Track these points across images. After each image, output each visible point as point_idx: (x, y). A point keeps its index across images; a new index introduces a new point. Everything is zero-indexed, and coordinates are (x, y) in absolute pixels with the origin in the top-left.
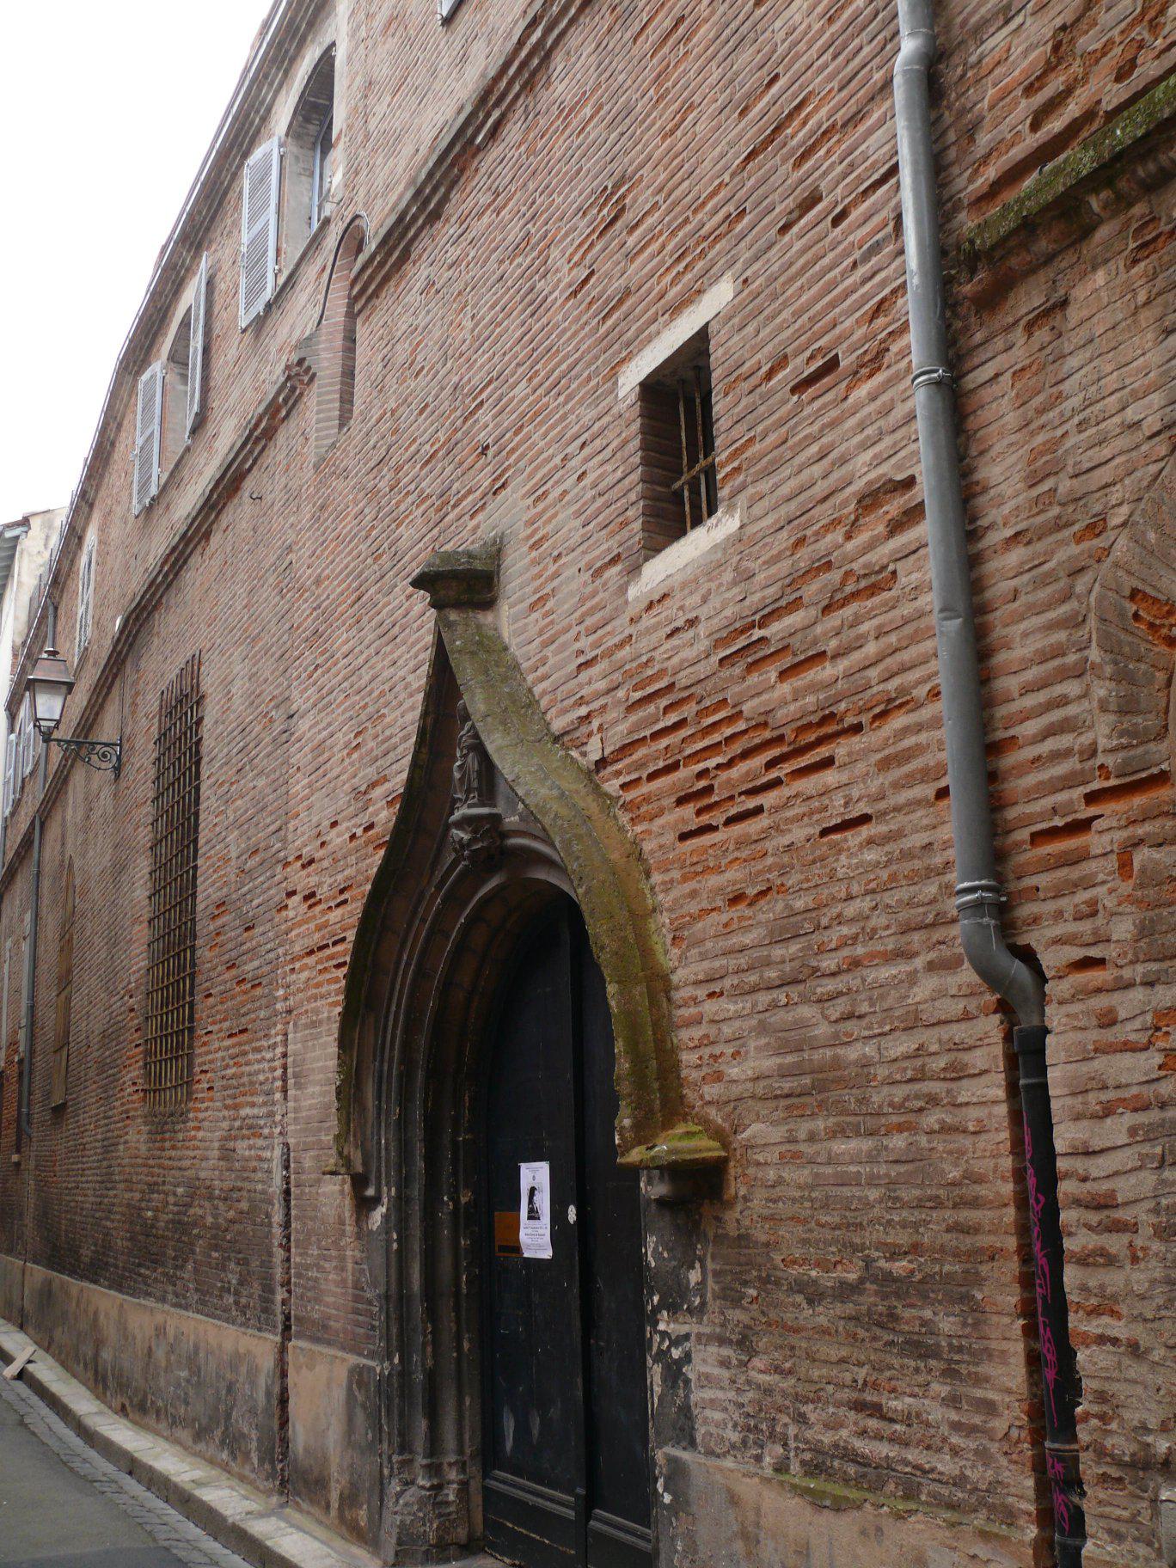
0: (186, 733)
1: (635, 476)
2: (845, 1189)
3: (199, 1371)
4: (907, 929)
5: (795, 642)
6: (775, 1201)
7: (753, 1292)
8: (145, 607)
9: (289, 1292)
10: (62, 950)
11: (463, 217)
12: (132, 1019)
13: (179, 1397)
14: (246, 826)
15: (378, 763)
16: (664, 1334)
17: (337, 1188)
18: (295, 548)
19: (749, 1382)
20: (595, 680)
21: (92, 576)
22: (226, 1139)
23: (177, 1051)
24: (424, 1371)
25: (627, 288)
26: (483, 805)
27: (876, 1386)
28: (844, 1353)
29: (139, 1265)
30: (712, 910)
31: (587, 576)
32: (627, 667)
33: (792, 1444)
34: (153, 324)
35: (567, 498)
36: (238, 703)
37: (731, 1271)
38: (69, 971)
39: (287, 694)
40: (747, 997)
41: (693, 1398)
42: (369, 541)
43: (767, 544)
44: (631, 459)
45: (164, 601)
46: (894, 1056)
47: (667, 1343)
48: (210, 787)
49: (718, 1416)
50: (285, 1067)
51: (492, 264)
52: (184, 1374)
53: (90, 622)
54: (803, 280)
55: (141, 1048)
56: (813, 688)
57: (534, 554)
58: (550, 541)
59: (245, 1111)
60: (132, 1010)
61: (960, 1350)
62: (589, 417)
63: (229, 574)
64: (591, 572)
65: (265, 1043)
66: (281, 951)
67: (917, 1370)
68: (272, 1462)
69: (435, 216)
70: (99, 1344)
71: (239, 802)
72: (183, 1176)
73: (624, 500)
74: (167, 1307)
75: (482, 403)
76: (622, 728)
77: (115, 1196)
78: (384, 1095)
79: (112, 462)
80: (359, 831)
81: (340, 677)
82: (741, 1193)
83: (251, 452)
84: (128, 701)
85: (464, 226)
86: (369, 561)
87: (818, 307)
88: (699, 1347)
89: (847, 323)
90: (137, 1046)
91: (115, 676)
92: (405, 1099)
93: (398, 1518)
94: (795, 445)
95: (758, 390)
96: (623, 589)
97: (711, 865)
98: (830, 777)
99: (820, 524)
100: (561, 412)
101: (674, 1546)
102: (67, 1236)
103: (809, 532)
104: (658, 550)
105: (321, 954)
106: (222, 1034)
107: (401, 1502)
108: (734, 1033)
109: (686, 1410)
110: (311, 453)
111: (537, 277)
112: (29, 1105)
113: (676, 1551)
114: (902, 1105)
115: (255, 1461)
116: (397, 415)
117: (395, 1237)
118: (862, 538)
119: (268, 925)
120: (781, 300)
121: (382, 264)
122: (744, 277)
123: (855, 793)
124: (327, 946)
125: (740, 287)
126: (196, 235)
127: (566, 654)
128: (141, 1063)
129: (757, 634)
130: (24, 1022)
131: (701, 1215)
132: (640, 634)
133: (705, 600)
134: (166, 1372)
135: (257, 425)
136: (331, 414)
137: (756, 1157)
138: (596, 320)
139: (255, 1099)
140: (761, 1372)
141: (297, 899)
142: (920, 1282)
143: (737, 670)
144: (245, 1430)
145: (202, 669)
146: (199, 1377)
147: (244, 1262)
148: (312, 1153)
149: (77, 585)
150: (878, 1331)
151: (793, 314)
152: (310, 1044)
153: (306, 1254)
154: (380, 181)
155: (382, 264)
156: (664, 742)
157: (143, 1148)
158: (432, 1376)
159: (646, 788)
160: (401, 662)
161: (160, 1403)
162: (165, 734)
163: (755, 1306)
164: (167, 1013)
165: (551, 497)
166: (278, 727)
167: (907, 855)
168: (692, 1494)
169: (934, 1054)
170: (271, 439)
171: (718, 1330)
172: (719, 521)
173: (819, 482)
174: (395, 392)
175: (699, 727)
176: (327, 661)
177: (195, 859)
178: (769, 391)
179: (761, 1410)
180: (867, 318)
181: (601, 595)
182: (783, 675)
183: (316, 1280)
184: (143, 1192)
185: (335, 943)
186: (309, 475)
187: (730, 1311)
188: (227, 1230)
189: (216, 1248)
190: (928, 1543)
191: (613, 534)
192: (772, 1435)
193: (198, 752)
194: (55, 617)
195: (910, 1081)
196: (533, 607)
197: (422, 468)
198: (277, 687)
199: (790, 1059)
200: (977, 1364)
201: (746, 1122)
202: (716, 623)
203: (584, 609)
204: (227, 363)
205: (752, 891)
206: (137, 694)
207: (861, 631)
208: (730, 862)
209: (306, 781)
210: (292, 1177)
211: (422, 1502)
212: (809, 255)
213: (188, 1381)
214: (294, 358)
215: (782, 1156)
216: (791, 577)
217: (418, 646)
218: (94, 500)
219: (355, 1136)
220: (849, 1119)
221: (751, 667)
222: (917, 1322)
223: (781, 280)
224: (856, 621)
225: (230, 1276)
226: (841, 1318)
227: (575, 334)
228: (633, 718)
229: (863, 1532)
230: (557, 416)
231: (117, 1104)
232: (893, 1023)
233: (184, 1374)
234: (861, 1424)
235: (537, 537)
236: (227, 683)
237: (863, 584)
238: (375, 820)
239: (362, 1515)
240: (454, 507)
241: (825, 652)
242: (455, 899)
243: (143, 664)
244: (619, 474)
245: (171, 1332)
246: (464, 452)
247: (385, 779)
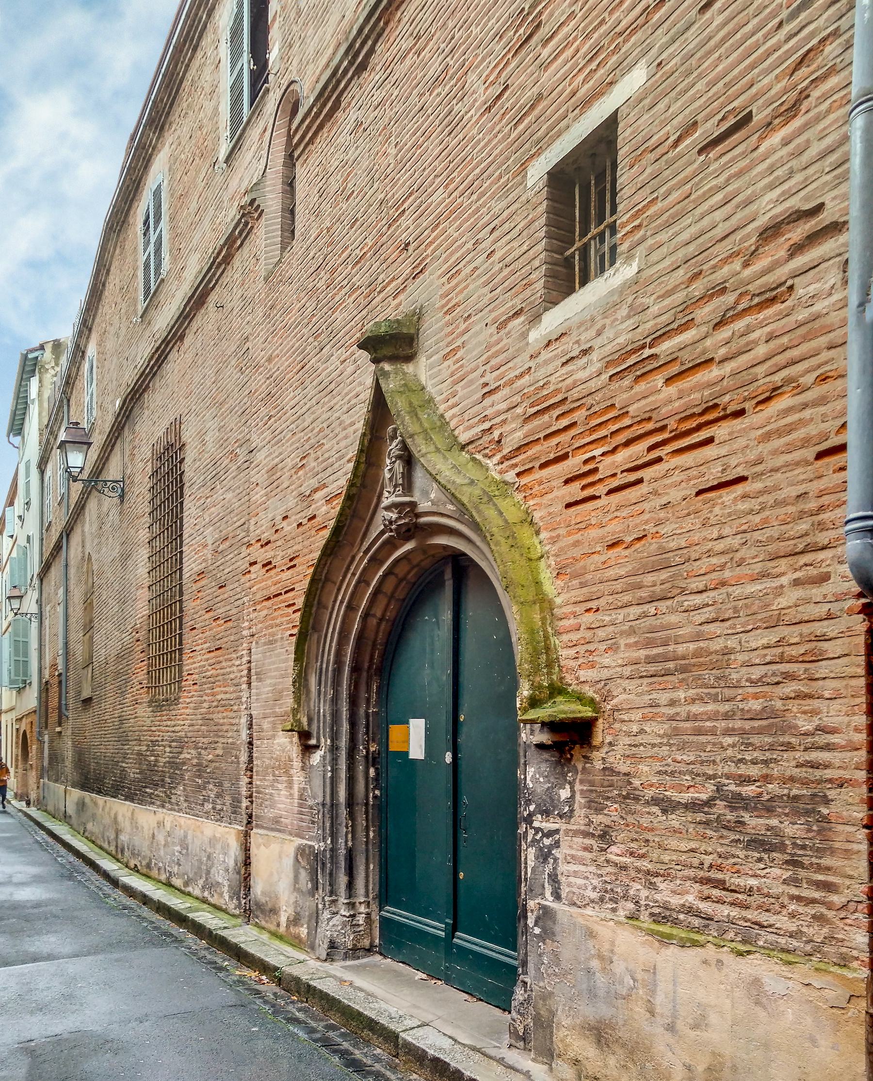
0: (172, 469)
5: (685, 355)
6: (635, 746)
8: (138, 390)
9: (252, 802)
10: (85, 609)
11: (387, 64)
12: (138, 646)
13: (174, 861)
14: (218, 524)
15: (319, 476)
16: (537, 830)
18: (251, 338)
19: (608, 861)
20: (498, 403)
21: (95, 377)
25: (540, 94)
27: (720, 868)
28: (693, 845)
31: (493, 329)
32: (525, 391)
34: (130, 192)
36: (211, 447)
38: (91, 621)
39: (248, 437)
40: (619, 611)
42: (310, 326)
43: (662, 282)
44: (537, 234)
45: (151, 385)
47: (540, 834)
50: (249, 670)
51: (414, 98)
53: (95, 406)
54: (722, 50)
55: (145, 663)
57: (448, 317)
58: (462, 307)
60: (138, 641)
61: (804, 847)
62: (499, 207)
63: (200, 362)
64: (496, 325)
65: (234, 656)
67: (760, 860)
68: (238, 899)
69: (363, 67)
70: (118, 832)
71: (213, 509)
73: (528, 267)
74: (165, 811)
75: (404, 211)
76: (519, 434)
77: (128, 749)
78: (323, 683)
79: (103, 297)
80: (305, 521)
81: (288, 423)
82: (607, 741)
83: (214, 275)
84: (127, 453)
85: (388, 71)
87: (736, 72)
88: (566, 838)
89: (766, 81)
91: (117, 438)
92: (336, 683)
93: (328, 933)
94: (699, 197)
95: (665, 158)
96: (524, 335)
98: (709, 452)
99: (719, 258)
100: (474, 208)
103: (705, 267)
104: (555, 303)
105: (276, 599)
106: (203, 652)
107: (331, 924)
108: (608, 635)
110: (262, 269)
111: (455, 102)
112: (66, 699)
114: (760, 680)
115: (227, 898)
116: (332, 231)
118: (758, 266)
119: (236, 585)
120: (695, 74)
121: (317, 115)
122: (659, 61)
124: (280, 594)
125: (655, 70)
126: (160, 120)
127: (474, 387)
128: (145, 671)
130: (61, 652)
131: (572, 755)
132: (538, 366)
133: (599, 334)
135: (219, 254)
136: (275, 240)
138: (509, 127)
139: (227, 689)
141: (258, 566)
142: (768, 800)
143: (626, 382)
144: (220, 881)
146: (187, 849)
147: (220, 785)
148: (269, 719)
149: (83, 384)
150: (725, 833)
151: (708, 84)
152: (268, 654)
154: (311, 50)
155: (317, 115)
160: (337, 407)
161: (161, 865)
162: (157, 471)
164: (163, 641)
165: (463, 274)
166: (241, 459)
170: (229, 264)
172: (617, 270)
173: (721, 225)
174: (329, 214)
175: (588, 427)
177: (181, 547)
178: (674, 158)
180: (789, 71)
181: (505, 341)
182: (669, 381)
183: (271, 795)
184: (148, 746)
185: (286, 592)
186: (261, 285)
189: (200, 777)
190: (765, 973)
191: (517, 295)
192: (625, 897)
193: (181, 481)
194: (69, 406)
196: (445, 357)
197: (353, 268)
198: (240, 433)
200: (821, 858)
201: (615, 694)
202: (608, 349)
203: (489, 353)
204: (189, 214)
205: (628, 539)
206: (134, 448)
209: (264, 492)
211: (344, 925)
212: (731, 26)
214: (247, 199)
216: (685, 305)
217: (351, 395)
218: (92, 325)
220: (706, 691)
221: (638, 379)
223: (698, 55)
224: (749, 330)
226: (691, 822)
227: (490, 141)
228: (526, 428)
230: (470, 211)
233: (178, 848)
235: (450, 306)
236: (201, 435)
237: (756, 300)
238: (317, 513)
239: (303, 931)
240: (380, 292)
241: (712, 359)
242: (376, 561)
243: (137, 428)
244: (525, 247)
245: (168, 826)
246: (390, 251)
247: (325, 486)
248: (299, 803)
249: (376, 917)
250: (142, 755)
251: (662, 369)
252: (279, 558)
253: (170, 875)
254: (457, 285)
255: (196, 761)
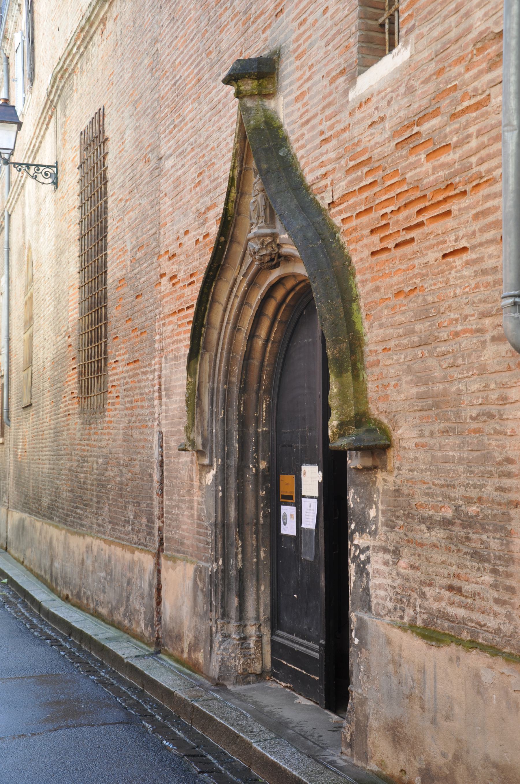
1: (355, 14)
2: (447, 465)
3: (111, 572)
4: (483, 315)
7: (401, 523)
10: (26, 303)
13: (100, 589)
15: (211, 195)
16: (357, 546)
17: (189, 459)
19: (398, 574)
22: (126, 428)
23: (98, 373)
24: (237, 569)
26: (268, 227)
27: (458, 577)
29: (77, 507)
30: (386, 299)
33: (418, 610)
35: (317, 25)
37: (390, 510)
38: (31, 318)
39: (158, 143)
41: (371, 583)
46: (473, 390)
47: (358, 551)
48: (113, 201)
49: (382, 593)
50: (160, 384)
52: (103, 574)
55: (76, 370)
56: (443, 166)
59: (137, 411)
64: (329, 78)
66: (157, 311)
68: (152, 626)
72: (102, 452)
76: (343, 183)
82: (397, 466)
86: (204, 55)
90: (74, 369)
91: (51, 117)
92: (227, 404)
96: (346, 93)
97: (387, 272)
98: (449, 223)
101: (359, 669)
102: (33, 490)
107: (222, 647)
108: (395, 373)
109: (366, 590)
113: (360, 671)
115: (143, 626)
117: (220, 488)
123: (461, 234)
124: (183, 309)
128: (76, 380)
129: (416, 129)
134: (92, 574)
137: (404, 445)
140: (404, 568)
141: (165, 279)
144: (137, 607)
145: (106, 119)
146: (111, 575)
150: (461, 547)
153: (171, 499)
156: (365, 194)
157: (78, 434)
158: (241, 573)
159: (354, 223)
161: (89, 593)
163: (402, 531)
166: (153, 165)
167: (484, 272)
168: (369, 638)
169: (492, 390)
171: (383, 544)
172: (399, 51)
176: (181, 122)
177: (106, 250)
179: (403, 590)
183: (177, 514)
187: (390, 533)
188: (127, 485)
193: (105, 178)
195: (481, 404)
199: (423, 389)
202: (396, 120)
205: (407, 289)
207: (469, 133)
208: (396, 271)
210: (164, 452)
213: (105, 579)
215: (417, 445)
219: (197, 427)
222: (479, 542)
224: (466, 126)
225: (130, 513)
229: (451, 660)
231: (62, 405)
232: (473, 371)
233: (103, 574)
234: (452, 599)
235: (300, 51)
238: (210, 231)
240: (253, 22)
241: (450, 144)
245: (95, 549)
248: (197, 523)
249: (267, 639)
250: (73, 471)
251: (424, 145)
252: (182, 273)
253: (97, 604)
254: (305, 32)
255: (118, 479)
